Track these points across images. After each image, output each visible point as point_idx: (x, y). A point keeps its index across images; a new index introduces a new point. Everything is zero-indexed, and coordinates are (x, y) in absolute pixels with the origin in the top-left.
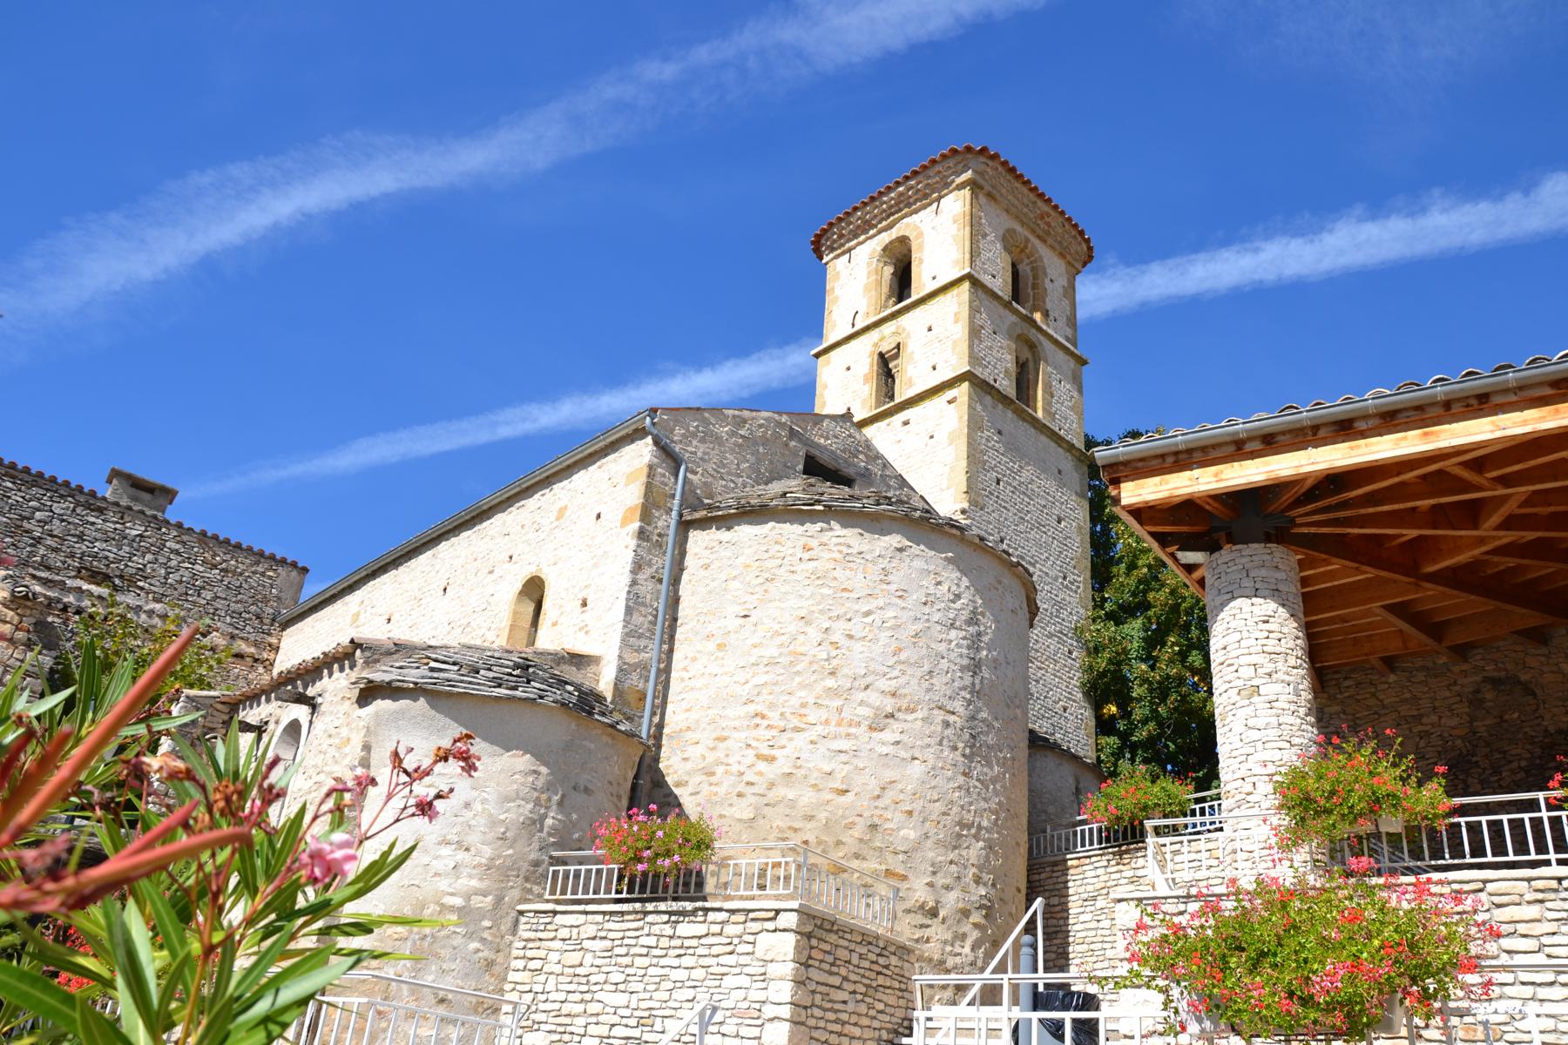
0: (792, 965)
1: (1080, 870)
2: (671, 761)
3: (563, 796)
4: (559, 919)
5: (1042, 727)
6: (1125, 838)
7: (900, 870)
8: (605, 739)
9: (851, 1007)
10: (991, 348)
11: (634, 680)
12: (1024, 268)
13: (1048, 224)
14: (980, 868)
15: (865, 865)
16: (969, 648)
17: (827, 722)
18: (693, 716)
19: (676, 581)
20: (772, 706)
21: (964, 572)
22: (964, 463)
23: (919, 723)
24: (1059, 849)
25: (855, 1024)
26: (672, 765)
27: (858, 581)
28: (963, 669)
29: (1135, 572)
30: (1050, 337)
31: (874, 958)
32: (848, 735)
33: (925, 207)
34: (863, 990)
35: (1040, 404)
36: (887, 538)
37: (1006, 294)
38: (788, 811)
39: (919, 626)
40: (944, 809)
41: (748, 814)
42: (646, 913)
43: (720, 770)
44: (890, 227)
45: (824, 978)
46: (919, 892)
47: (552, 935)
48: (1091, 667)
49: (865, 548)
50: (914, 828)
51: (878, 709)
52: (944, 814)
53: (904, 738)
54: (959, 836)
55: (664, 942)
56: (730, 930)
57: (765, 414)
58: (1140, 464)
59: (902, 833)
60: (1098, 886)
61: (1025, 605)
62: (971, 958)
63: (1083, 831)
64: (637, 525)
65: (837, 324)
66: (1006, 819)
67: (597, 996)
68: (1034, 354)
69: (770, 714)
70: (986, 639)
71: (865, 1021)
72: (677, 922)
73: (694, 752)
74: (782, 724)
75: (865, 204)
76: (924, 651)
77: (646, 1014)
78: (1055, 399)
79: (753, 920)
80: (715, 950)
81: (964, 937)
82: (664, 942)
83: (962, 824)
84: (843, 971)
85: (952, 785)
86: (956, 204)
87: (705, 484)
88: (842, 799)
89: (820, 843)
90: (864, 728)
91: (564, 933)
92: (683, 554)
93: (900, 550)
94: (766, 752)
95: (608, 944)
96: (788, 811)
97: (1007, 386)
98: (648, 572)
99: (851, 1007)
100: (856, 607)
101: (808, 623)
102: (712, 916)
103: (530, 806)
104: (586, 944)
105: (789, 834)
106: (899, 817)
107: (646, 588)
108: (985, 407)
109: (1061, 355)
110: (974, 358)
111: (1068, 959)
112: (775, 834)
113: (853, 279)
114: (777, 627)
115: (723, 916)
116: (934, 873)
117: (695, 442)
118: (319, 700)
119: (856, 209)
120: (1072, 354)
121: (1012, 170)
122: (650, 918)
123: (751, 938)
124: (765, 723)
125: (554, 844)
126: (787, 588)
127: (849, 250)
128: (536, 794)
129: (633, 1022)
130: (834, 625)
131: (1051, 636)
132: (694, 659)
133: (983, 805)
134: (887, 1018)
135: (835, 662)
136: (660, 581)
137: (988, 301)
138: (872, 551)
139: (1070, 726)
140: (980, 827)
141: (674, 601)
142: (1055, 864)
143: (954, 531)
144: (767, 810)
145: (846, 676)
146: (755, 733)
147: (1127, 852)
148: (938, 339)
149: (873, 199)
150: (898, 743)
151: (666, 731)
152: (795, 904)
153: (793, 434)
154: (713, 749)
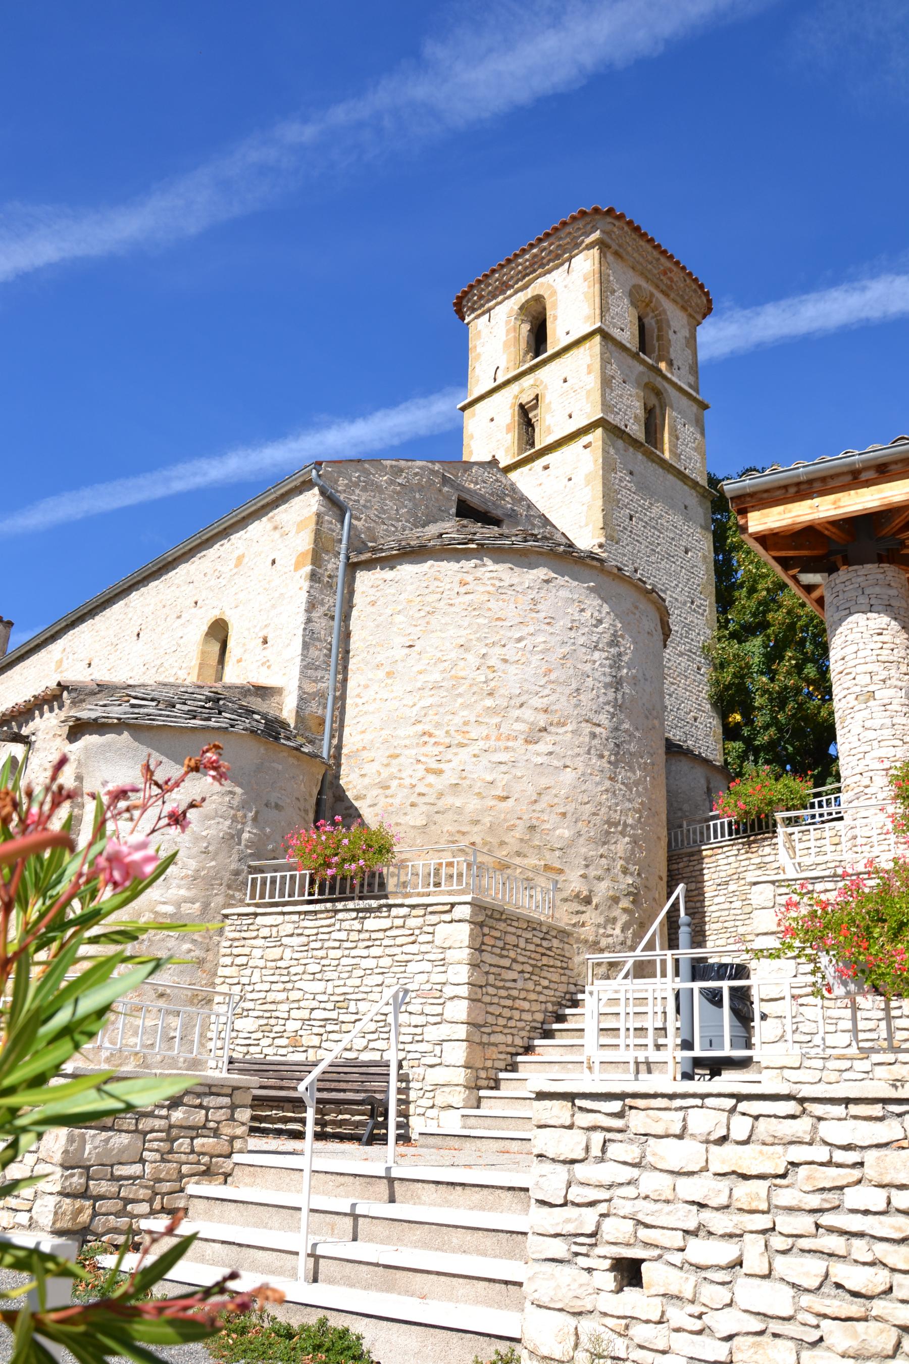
0: (468, 951)
1: (713, 859)
2: (350, 778)
3: (257, 813)
5: (676, 735)
6: (752, 829)
7: (557, 865)
8: (291, 760)
9: (520, 984)
10: (621, 396)
11: (314, 707)
12: (650, 321)
13: (671, 279)
14: (627, 860)
16: (611, 667)
17: (487, 737)
18: (368, 737)
19: (346, 617)
20: (438, 725)
21: (604, 600)
22: (600, 502)
23: (569, 735)
24: (695, 842)
25: (524, 999)
26: (352, 781)
27: (510, 611)
31: (538, 941)
32: (507, 748)
33: (557, 267)
34: (530, 969)
35: (666, 446)
36: (535, 571)
37: (633, 345)
38: (456, 817)
39: (566, 649)
40: (594, 810)
42: (337, 911)
43: (394, 784)
44: (525, 287)
46: (574, 883)
47: (254, 934)
48: (717, 681)
49: (515, 580)
50: (568, 827)
51: (532, 724)
52: (594, 814)
53: (557, 749)
54: (608, 833)
55: (354, 936)
56: (412, 922)
57: (419, 463)
58: (765, 495)
59: (557, 832)
62: (621, 938)
65: (480, 379)
66: (648, 817)
68: (660, 400)
69: (437, 733)
70: (626, 658)
71: (533, 996)
72: (365, 918)
74: (447, 741)
75: (502, 266)
76: (571, 672)
78: (681, 442)
79: (431, 913)
80: (399, 941)
81: (614, 920)
82: (354, 936)
83: (609, 823)
84: (512, 954)
85: (600, 788)
86: (585, 263)
87: (368, 528)
88: (504, 805)
90: (520, 741)
91: (265, 932)
92: (351, 592)
93: (547, 581)
94: (435, 766)
95: (304, 940)
96: (456, 817)
99: (520, 984)
100: (509, 634)
101: (467, 650)
103: (228, 822)
104: (285, 941)
106: (554, 818)
107: (321, 624)
108: (617, 451)
109: (684, 402)
110: (606, 406)
111: (705, 936)
112: (446, 837)
113: (493, 336)
114: (439, 655)
115: (404, 911)
116: (587, 866)
117: (357, 491)
118: (33, 738)
119: (493, 271)
120: (694, 399)
121: (637, 229)
122: (340, 916)
123: (430, 929)
124: (433, 740)
125: (251, 855)
127: (489, 310)
128: (232, 812)
131: (681, 654)
132: (366, 687)
133: (628, 805)
134: (552, 993)
135: (492, 684)
136: (332, 618)
137: (617, 353)
138: (521, 583)
139: (700, 734)
140: (625, 825)
141: (346, 636)
142: (692, 854)
143: (595, 563)
144: (437, 817)
146: (424, 750)
147: (754, 842)
148: (573, 390)
149: (509, 261)
150: (551, 753)
151: (345, 751)
152: (468, 898)
153: (445, 480)
154: (387, 765)
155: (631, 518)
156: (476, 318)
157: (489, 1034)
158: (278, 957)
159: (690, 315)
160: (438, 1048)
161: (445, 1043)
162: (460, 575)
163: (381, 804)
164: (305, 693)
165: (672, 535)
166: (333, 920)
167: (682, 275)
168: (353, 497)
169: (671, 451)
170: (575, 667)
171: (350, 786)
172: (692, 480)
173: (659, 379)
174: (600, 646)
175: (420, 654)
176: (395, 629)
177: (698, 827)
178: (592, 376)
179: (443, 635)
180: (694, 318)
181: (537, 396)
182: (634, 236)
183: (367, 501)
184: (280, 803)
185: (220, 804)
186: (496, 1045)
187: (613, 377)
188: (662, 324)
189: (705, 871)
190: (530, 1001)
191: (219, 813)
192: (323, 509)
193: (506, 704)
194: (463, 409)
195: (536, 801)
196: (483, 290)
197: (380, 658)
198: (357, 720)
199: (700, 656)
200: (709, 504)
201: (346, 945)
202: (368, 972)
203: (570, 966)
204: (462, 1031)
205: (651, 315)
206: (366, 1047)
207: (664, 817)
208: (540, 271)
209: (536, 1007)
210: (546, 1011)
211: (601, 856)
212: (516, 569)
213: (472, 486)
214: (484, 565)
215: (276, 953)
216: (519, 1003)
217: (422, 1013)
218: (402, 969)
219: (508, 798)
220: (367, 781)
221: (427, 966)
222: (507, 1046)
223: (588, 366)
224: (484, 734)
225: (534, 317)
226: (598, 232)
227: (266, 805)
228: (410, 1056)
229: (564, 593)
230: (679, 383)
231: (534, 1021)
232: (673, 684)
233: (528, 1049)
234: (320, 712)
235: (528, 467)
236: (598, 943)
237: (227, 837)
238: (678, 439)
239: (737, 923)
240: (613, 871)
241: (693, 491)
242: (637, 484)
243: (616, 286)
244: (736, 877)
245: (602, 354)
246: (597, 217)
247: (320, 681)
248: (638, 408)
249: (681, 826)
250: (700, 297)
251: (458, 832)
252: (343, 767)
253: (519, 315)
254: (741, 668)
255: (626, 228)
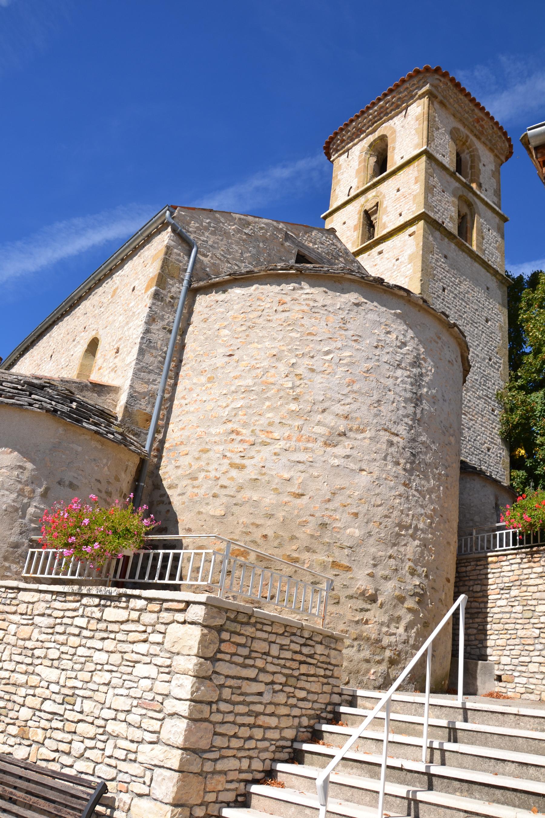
0: (195, 660)
1: (498, 565)
2: (168, 468)
3: (47, 490)
4: (23, 596)
5: (472, 460)
6: (535, 541)
7: (345, 562)
8: (94, 444)
9: (266, 698)
10: (440, 201)
11: (142, 405)
12: (465, 156)
13: (482, 126)
14: (416, 562)
15: (315, 557)
16: (412, 384)
17: (289, 438)
18: (186, 433)
19: (183, 332)
20: (245, 425)
21: (410, 326)
22: (419, 275)
23: (367, 441)
24: (482, 548)
25: (272, 714)
26: (169, 472)
27: (321, 328)
28: (406, 400)
29: (540, 356)
30: (482, 200)
31: (297, 648)
32: (306, 449)
33: (397, 115)
34: (283, 680)
35: (474, 243)
36: (347, 295)
37: (452, 167)
38: (252, 510)
39: (369, 365)
41: (220, 512)
42: (83, 595)
43: (202, 475)
44: (374, 131)
45: (235, 671)
46: (361, 581)
47: (13, 609)
48: (508, 421)
49: (328, 302)
50: (359, 527)
51: (332, 428)
52: (386, 516)
53: (354, 453)
54: (398, 535)
55: (93, 625)
56: (148, 618)
57: (265, 220)
59: (348, 531)
60: (512, 578)
61: (460, 360)
62: (404, 637)
63: (501, 535)
64: (154, 289)
65: (338, 196)
66: (439, 523)
67: (38, 669)
68: (471, 210)
69: (244, 431)
70: (427, 379)
71: (283, 710)
72: (105, 606)
73: (184, 461)
74: (252, 439)
75: (358, 117)
76: (374, 384)
77: (70, 692)
78: (485, 238)
79: (167, 610)
80: (133, 637)
81: (399, 619)
82: (93, 625)
83: (401, 526)
84: (260, 663)
85: (393, 493)
86: (418, 109)
87: (214, 264)
88: (298, 501)
89: (277, 537)
90: (320, 443)
91: (22, 608)
92: (191, 312)
93: (357, 305)
94: (238, 461)
95: (51, 621)
96: (252, 510)
97: (452, 227)
98: (160, 324)
99: (266, 698)
100: (318, 348)
101: (279, 360)
102: (134, 603)
103: (14, 496)
104: (37, 620)
105: (252, 529)
106: (346, 517)
107: (158, 336)
108: (435, 239)
109: (489, 213)
110: (427, 204)
111: (486, 635)
112: (241, 528)
113: (349, 169)
114: (254, 363)
115: (141, 603)
116: (375, 566)
117: (207, 234)
119: (352, 121)
120: (497, 213)
122: (85, 601)
123: (161, 628)
124: (239, 438)
125: (34, 529)
126: (264, 333)
127: (348, 150)
128: (20, 486)
129: (59, 698)
130: (299, 361)
131: (479, 398)
132: (191, 390)
133: (420, 510)
134: (309, 705)
135: (298, 390)
136: (170, 331)
137: (438, 170)
138: (333, 305)
139: (492, 461)
140: (416, 529)
141: (180, 348)
142: (479, 559)
143: (402, 293)
144: (235, 509)
145: (307, 401)
146: (230, 446)
147: (537, 552)
148: (403, 197)
149: (363, 113)
150: (348, 457)
151: (167, 445)
152: (202, 598)
153: (287, 237)
154: (198, 459)
155: (444, 290)
156: (339, 156)
157: (215, 760)
158: (27, 636)
159: (496, 156)
160: (148, 773)
161: (157, 771)
162: (279, 297)
163: (188, 494)
164: (135, 392)
165: (476, 307)
166: (78, 604)
167: (491, 124)
168: (202, 238)
169: (477, 246)
170: (377, 381)
171: (167, 476)
172: (494, 269)
173: (471, 194)
174: (403, 365)
175: (238, 361)
176: (220, 341)
177: (486, 535)
178: (418, 185)
179: (260, 346)
180: (499, 158)
181: (377, 203)
182: (455, 91)
183: (214, 242)
184: (75, 482)
185: (8, 477)
186: (225, 773)
187: (434, 187)
188: (475, 158)
189: (490, 576)
190: (279, 717)
191: (6, 486)
192: (173, 243)
193: (309, 408)
194: (325, 218)
195: (329, 500)
196: (344, 135)
197: (204, 365)
198: (180, 418)
199: (494, 401)
200: (506, 289)
201: (85, 633)
202: (99, 667)
203: (336, 675)
204: (175, 758)
205: (467, 151)
206: (82, 755)
207: (455, 525)
208: (385, 118)
209: (285, 722)
210: (300, 725)
211: (390, 557)
212: (330, 292)
213: (311, 245)
214: (302, 288)
215: (25, 631)
216: (262, 720)
217: (139, 727)
218: (129, 670)
219: (303, 495)
220: (180, 472)
221: (152, 671)
222: (241, 771)
223: (416, 178)
224: (286, 435)
225: (379, 153)
226: (428, 85)
227: (59, 483)
228: (121, 777)
229: (371, 316)
230: (486, 199)
231: (283, 739)
232: (471, 420)
233: (269, 776)
234: (148, 410)
235: (368, 253)
236: (380, 641)
237: (9, 509)
238: (483, 239)
239: (518, 626)
240: (400, 572)
241: (493, 278)
242: (451, 266)
243: (440, 126)
244: (518, 583)
245: (426, 169)
246: (428, 74)
247: (151, 383)
248: (453, 211)
249: (471, 534)
250: (504, 142)
251: (253, 524)
252: (163, 460)
253: (368, 151)
254: (527, 411)
255: (449, 84)
